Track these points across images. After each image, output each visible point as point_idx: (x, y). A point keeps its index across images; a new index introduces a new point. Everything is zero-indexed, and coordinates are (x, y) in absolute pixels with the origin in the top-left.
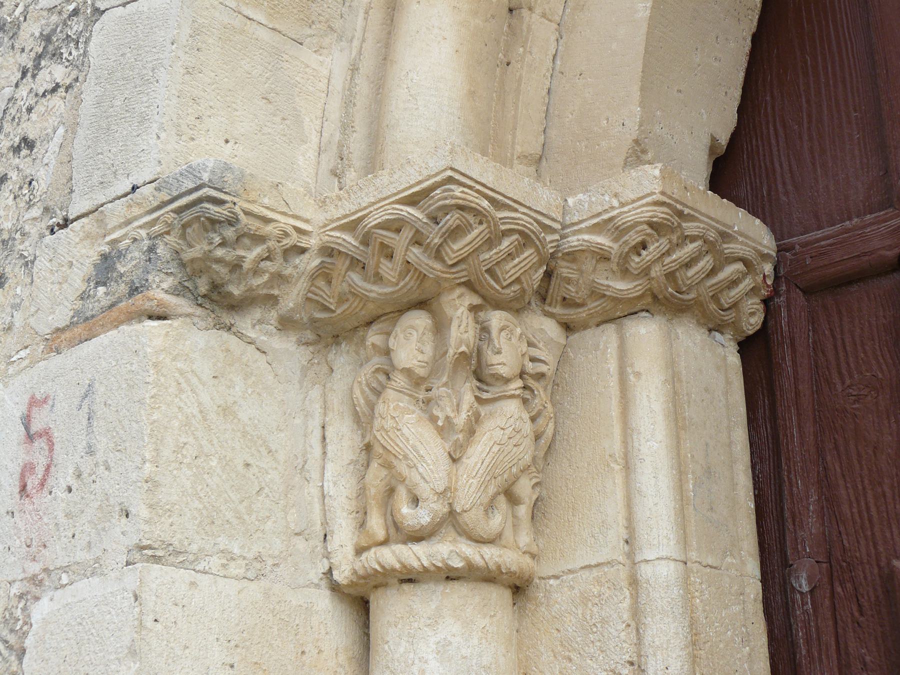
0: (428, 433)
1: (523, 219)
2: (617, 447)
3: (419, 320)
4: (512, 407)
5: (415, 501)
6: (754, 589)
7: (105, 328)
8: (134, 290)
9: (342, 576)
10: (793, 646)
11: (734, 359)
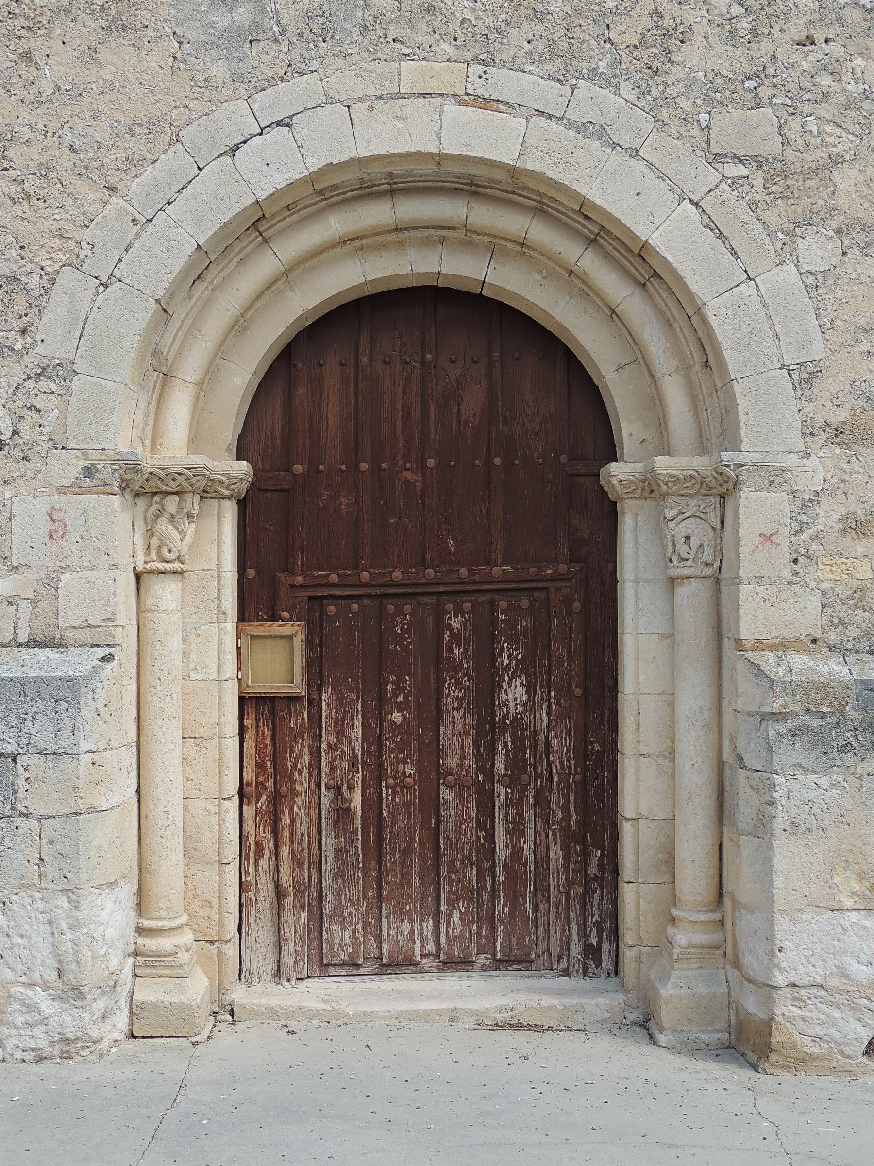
3: (176, 498)
5: (170, 551)
7: (90, 493)
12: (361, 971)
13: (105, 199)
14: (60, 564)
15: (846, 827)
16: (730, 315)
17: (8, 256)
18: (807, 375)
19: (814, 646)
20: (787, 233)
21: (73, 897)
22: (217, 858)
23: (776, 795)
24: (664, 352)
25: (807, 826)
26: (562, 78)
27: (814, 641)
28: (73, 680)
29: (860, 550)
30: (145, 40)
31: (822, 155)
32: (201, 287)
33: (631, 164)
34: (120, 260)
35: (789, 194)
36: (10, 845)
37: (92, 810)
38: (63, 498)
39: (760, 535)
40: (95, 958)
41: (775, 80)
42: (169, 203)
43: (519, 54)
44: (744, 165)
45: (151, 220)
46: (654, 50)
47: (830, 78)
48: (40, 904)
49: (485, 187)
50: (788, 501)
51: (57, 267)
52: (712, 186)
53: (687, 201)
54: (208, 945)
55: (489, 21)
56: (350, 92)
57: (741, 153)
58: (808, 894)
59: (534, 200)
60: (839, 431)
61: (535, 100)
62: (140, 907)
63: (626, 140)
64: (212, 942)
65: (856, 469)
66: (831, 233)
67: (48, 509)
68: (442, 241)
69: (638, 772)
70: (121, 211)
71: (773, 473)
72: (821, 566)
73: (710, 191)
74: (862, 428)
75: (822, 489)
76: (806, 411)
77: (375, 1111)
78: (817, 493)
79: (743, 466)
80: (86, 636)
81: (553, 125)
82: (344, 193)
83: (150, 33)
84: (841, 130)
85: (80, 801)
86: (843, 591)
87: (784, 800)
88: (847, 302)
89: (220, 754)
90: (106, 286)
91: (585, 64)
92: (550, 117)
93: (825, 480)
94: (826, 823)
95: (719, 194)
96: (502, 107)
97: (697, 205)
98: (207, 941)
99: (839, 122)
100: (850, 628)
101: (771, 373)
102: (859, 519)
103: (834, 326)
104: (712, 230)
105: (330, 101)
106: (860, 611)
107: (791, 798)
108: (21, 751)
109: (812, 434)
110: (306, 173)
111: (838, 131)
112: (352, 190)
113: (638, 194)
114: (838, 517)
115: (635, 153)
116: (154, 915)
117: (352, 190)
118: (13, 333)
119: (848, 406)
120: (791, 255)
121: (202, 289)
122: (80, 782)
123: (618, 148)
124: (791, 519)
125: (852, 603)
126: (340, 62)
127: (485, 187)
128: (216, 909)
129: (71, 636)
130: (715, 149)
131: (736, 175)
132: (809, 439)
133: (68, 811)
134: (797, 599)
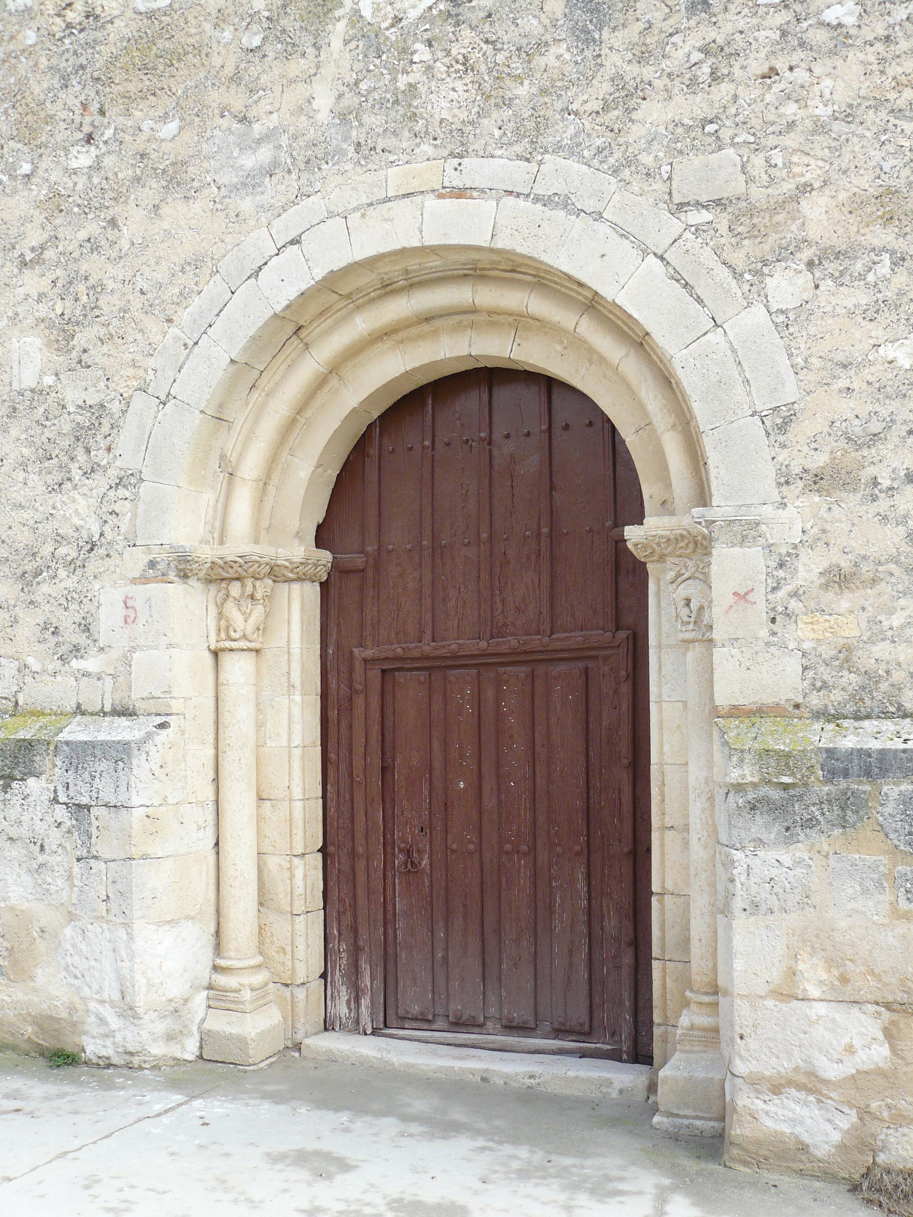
0: (239, 614)
1: (267, 560)
2: (286, 617)
3: (237, 584)
4: (260, 607)
5: (235, 631)
6: (319, 652)
7: (153, 582)
8: (163, 575)
9: (212, 648)
10: (326, 667)
11: (318, 589)
12: (434, 1027)
13: (164, 330)
14: (132, 644)
15: (812, 909)
16: (698, 366)
17: (99, 388)
18: (781, 420)
19: (797, 711)
20: (756, 273)
21: (129, 930)
22: (289, 909)
23: (735, 872)
24: (661, 409)
25: (769, 906)
26: (528, 156)
27: (797, 706)
28: (127, 743)
29: (844, 605)
30: (193, 191)
31: (789, 186)
32: (255, 394)
33: (595, 227)
34: (175, 381)
35: (756, 233)
36: (86, 882)
37: (145, 857)
38: (134, 587)
39: (734, 594)
40: (150, 985)
41: (737, 119)
42: (210, 326)
43: (491, 141)
44: (707, 210)
45: (196, 343)
46: (616, 113)
47: (795, 106)
48: (107, 934)
49: (489, 269)
50: (763, 556)
51: (130, 392)
52: (676, 236)
53: (652, 255)
54: (283, 987)
55: (463, 115)
56: (346, 204)
57: (703, 199)
58: (769, 980)
59: (531, 275)
60: (818, 478)
61: (505, 182)
62: (218, 948)
63: (589, 205)
64: (287, 985)
65: (837, 516)
66: (802, 267)
67: (123, 598)
68: (472, 325)
69: (662, 846)
70: (177, 339)
71: (746, 527)
72: (800, 625)
73: (673, 243)
74: (843, 471)
75: (801, 542)
76: (780, 458)
77: (19, 1108)
78: (795, 547)
79: (715, 522)
80: (151, 706)
81: (521, 202)
82: (368, 294)
83: (196, 184)
84: (809, 158)
85: (133, 848)
86: (827, 652)
87: (743, 878)
88: (822, 338)
89: (290, 814)
90: (164, 404)
91: (550, 139)
92: (518, 195)
93: (803, 532)
94: (789, 904)
95: (683, 243)
96: (475, 194)
97: (662, 258)
98: (283, 984)
99: (807, 149)
100: (834, 692)
101: (741, 421)
102: (843, 571)
103: (808, 365)
104: (677, 281)
105: (331, 215)
106: (845, 673)
107: (751, 875)
108: (93, 803)
109: (787, 483)
110: (313, 282)
111: (806, 160)
112: (375, 290)
113: (603, 256)
114: (820, 571)
115: (598, 216)
116: (226, 954)
117: (375, 290)
118: (101, 451)
119: (828, 449)
120: (759, 295)
121: (256, 396)
122: (133, 831)
123: (583, 214)
124: (767, 575)
125: (837, 663)
126: (339, 180)
127: (489, 269)
128: (289, 956)
129: (140, 706)
130: (677, 199)
131: (699, 221)
132: (784, 488)
133: (122, 856)
134: (775, 661)
